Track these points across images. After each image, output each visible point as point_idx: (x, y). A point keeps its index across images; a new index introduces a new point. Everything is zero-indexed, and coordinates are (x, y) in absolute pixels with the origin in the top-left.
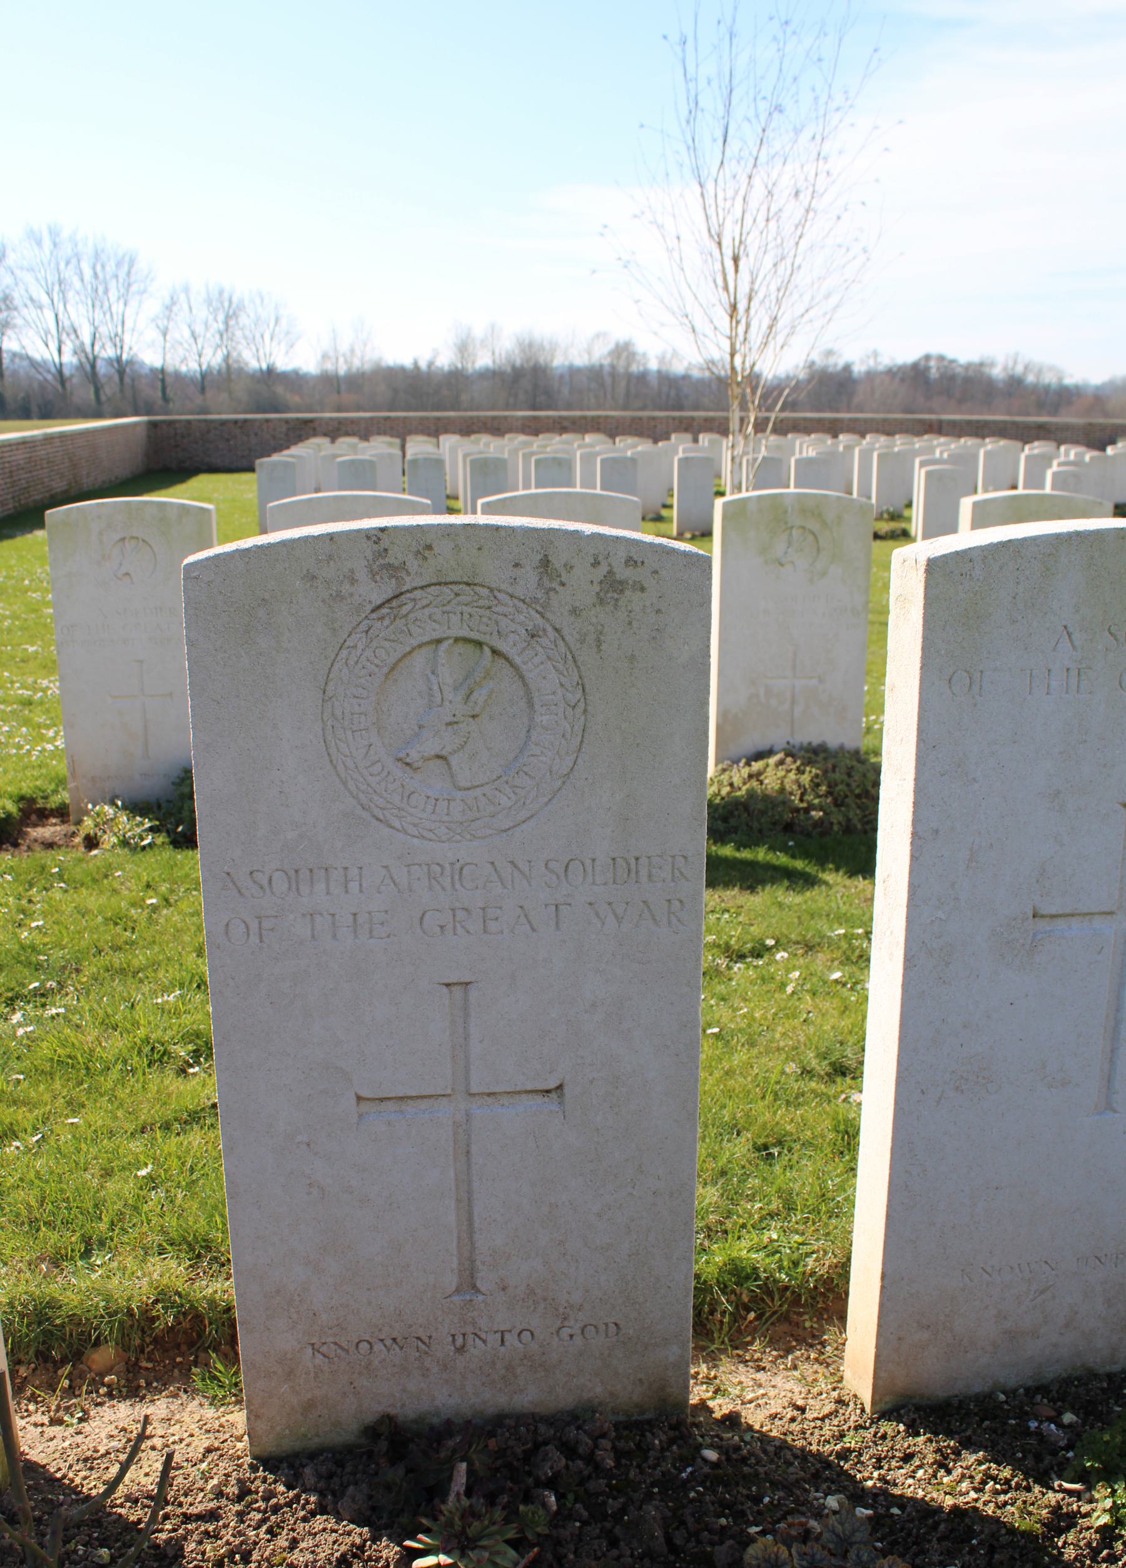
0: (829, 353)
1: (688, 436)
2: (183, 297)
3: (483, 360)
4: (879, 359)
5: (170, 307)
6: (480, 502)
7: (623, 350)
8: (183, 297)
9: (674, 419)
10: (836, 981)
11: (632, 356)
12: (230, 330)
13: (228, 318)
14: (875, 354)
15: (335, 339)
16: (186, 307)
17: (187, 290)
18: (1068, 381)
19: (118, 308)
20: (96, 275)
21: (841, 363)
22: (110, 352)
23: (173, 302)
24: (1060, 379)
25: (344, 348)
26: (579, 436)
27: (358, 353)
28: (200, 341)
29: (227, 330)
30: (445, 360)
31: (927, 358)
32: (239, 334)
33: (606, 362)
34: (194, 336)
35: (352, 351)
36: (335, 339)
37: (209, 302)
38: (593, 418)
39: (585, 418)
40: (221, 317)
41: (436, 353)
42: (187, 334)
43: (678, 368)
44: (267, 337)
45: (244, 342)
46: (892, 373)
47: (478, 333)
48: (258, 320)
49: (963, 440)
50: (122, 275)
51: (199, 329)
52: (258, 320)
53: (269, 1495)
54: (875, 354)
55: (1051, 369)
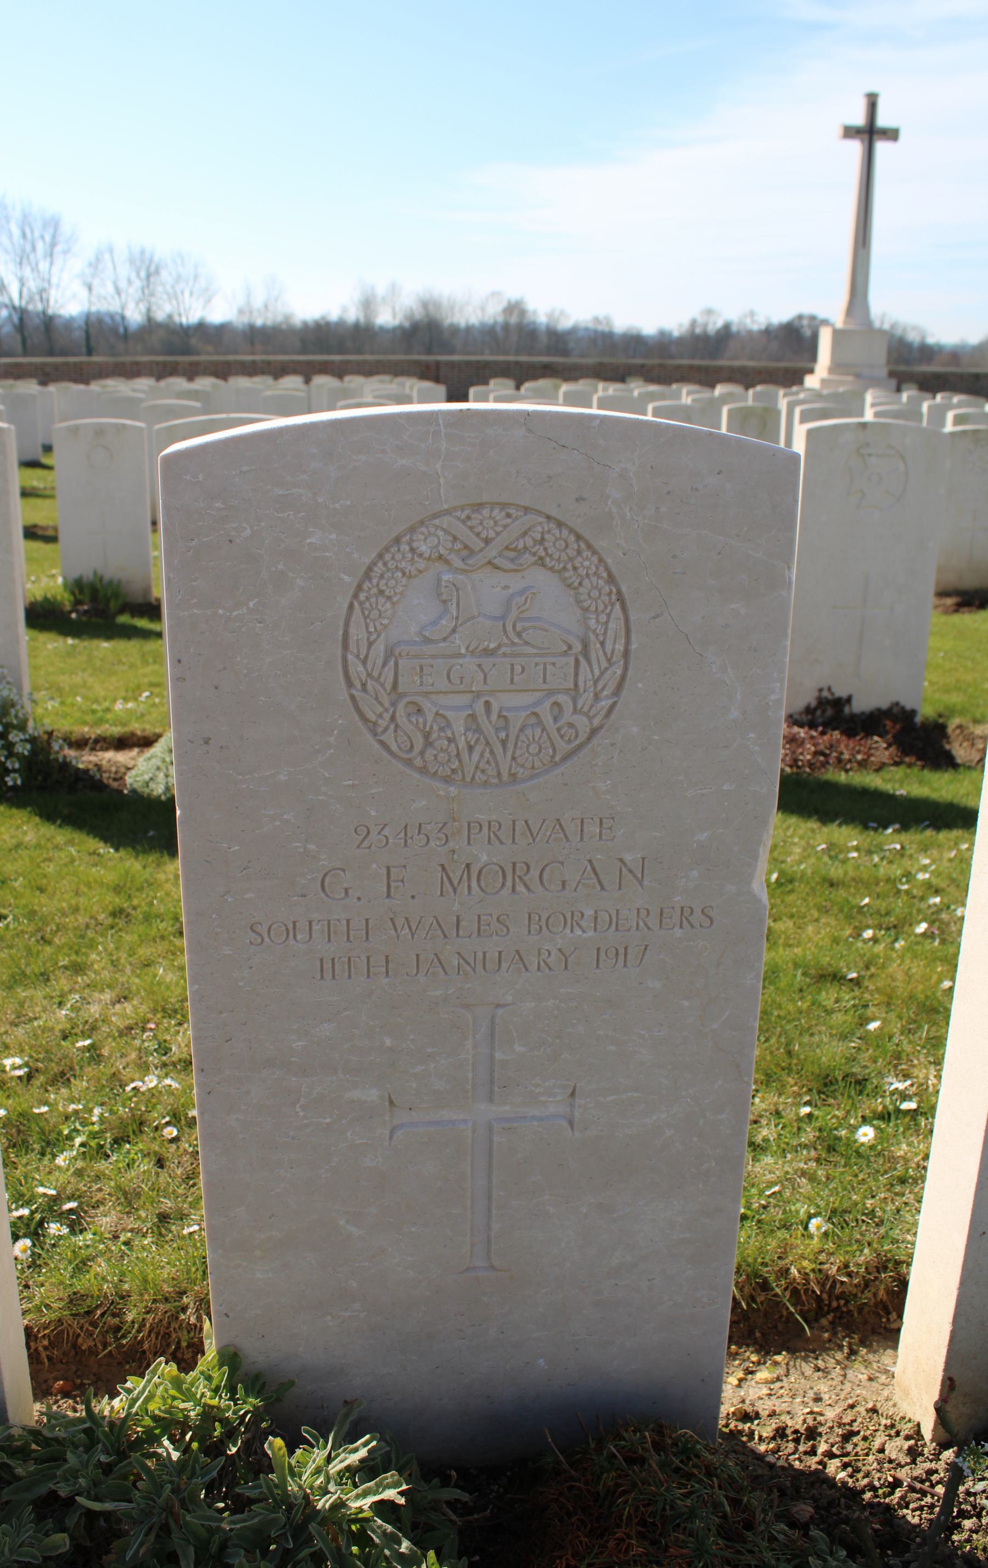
0: (709, 312)
1: (511, 383)
2: (107, 256)
3: (385, 318)
4: (756, 318)
5: (96, 265)
6: (797, 411)
7: (515, 308)
8: (107, 256)
9: (158, 363)
10: (924, 935)
11: (523, 313)
12: (151, 286)
13: (148, 276)
14: (752, 314)
15: (249, 296)
16: (110, 266)
17: (111, 251)
18: (930, 340)
19: (43, 266)
20: (24, 236)
21: (720, 324)
22: (40, 307)
23: (98, 260)
24: (923, 338)
25: (258, 303)
26: (929, 395)
27: (270, 308)
28: (123, 296)
29: (148, 286)
30: (353, 315)
31: (800, 317)
32: (160, 289)
33: (500, 319)
34: (118, 292)
35: (266, 307)
36: (249, 296)
37: (131, 261)
38: (75, 364)
39: (67, 364)
40: (143, 274)
41: (345, 310)
42: (110, 289)
43: (565, 324)
44: (187, 294)
45: (165, 297)
46: (768, 332)
47: (381, 291)
48: (179, 278)
49: (939, 397)
50: (48, 238)
51: (123, 284)
52: (179, 278)
53: (185, 1201)
54: (752, 314)
55: (915, 328)
